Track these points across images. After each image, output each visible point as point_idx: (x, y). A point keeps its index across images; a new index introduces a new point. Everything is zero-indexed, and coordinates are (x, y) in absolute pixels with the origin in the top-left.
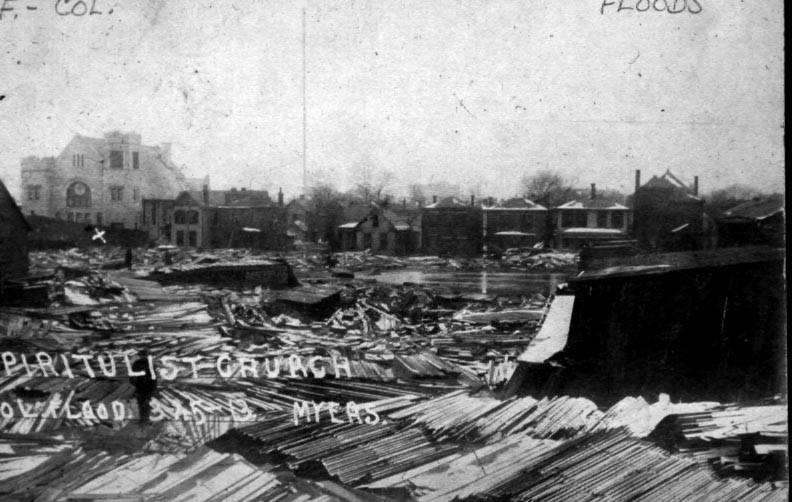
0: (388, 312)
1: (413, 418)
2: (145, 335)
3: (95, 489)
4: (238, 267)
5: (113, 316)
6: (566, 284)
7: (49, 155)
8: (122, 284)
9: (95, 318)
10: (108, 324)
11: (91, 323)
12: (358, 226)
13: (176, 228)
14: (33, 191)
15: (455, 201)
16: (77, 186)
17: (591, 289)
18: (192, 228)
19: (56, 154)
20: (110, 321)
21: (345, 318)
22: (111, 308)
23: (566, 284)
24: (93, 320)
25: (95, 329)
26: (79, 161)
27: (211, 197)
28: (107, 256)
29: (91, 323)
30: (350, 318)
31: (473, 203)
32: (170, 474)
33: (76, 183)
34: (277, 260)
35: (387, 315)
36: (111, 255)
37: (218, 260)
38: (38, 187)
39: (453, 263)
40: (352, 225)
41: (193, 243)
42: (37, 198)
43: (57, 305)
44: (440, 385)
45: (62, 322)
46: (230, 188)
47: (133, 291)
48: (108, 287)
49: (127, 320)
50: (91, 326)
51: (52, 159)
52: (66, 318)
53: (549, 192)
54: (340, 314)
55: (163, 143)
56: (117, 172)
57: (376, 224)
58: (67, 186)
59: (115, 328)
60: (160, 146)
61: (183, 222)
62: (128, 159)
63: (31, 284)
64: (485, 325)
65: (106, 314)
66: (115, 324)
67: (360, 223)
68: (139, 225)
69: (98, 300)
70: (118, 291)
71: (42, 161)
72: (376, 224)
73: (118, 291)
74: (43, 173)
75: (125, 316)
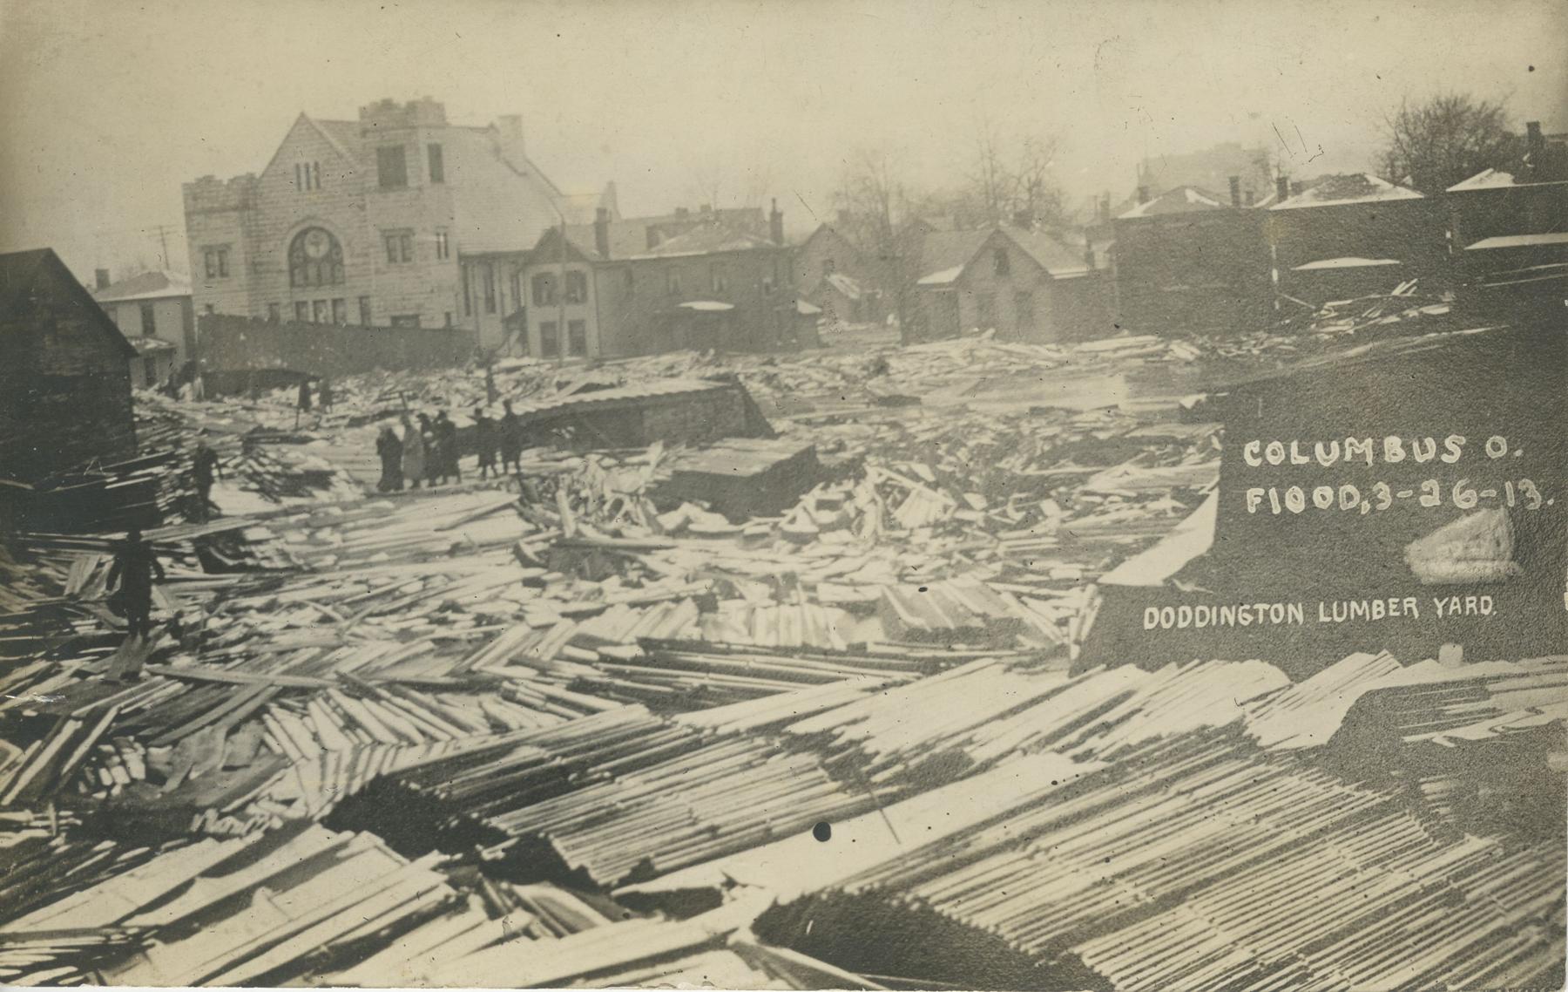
0: (928, 485)
1: (836, 732)
2: (356, 575)
3: (1050, 894)
4: (625, 399)
5: (294, 536)
6: (1203, 397)
7: (242, 170)
8: (330, 463)
9: (259, 542)
10: (284, 555)
11: (251, 555)
12: (961, 280)
13: (536, 317)
14: (215, 259)
15: (1192, 196)
16: (310, 236)
17: (29, 487)
18: (573, 312)
19: (258, 169)
20: (288, 548)
21: (821, 505)
22: (292, 519)
23: (1203, 397)
24: (253, 548)
25: (257, 569)
26: (310, 177)
27: (614, 234)
28: (366, 398)
29: (251, 555)
30: (830, 505)
31: (1236, 202)
32: (198, 879)
33: (304, 232)
34: (719, 378)
35: (928, 492)
36: (376, 394)
37: (621, 384)
38: (224, 250)
39: (1183, 350)
40: (948, 276)
41: (579, 347)
42: (223, 274)
43: (178, 520)
44: (961, 649)
45: (179, 558)
46: (672, 211)
47: (358, 475)
48: (297, 470)
49: (324, 543)
50: (249, 561)
51: (251, 177)
52: (188, 548)
53: (682, 212)
54: (809, 500)
55: (502, 118)
56: (392, 196)
57: (1003, 268)
58: (288, 241)
59: (301, 562)
60: (498, 123)
61: (551, 301)
62: (418, 166)
63: (123, 473)
64: (1157, 497)
65: (278, 532)
66: (298, 555)
67: (969, 268)
68: (454, 321)
69: (277, 501)
70: (321, 479)
71: (228, 187)
72: (1003, 268)
73: (321, 479)
74: (234, 215)
75: (324, 534)
